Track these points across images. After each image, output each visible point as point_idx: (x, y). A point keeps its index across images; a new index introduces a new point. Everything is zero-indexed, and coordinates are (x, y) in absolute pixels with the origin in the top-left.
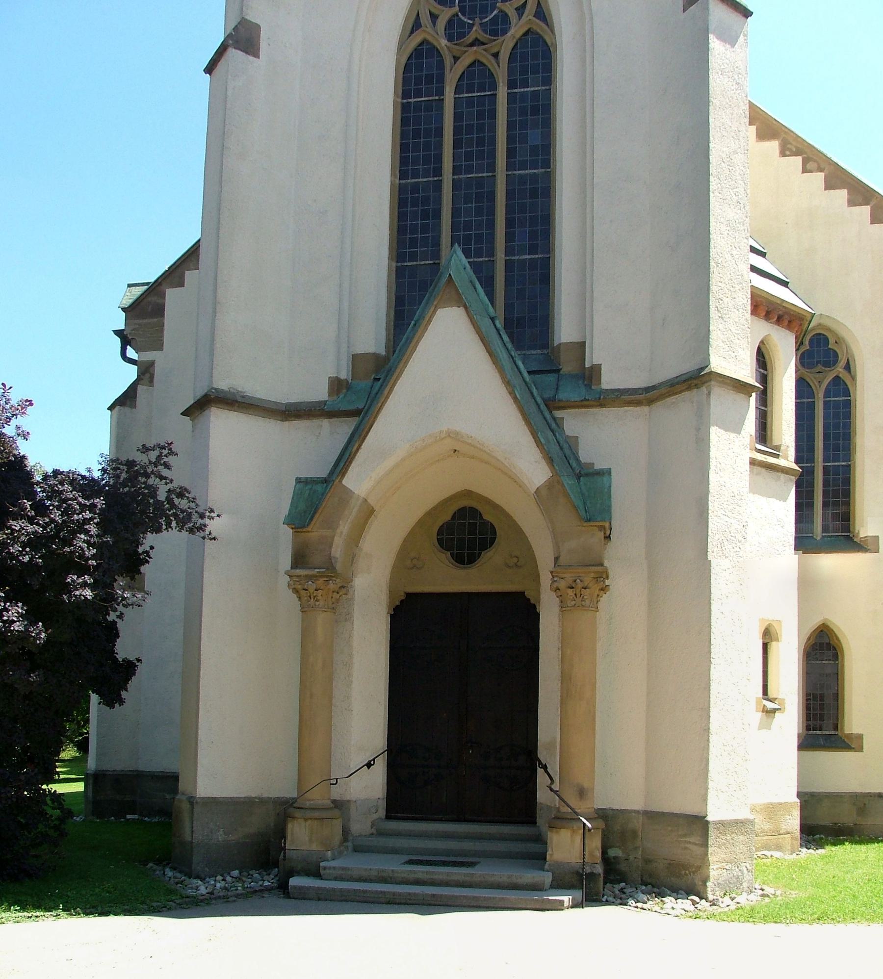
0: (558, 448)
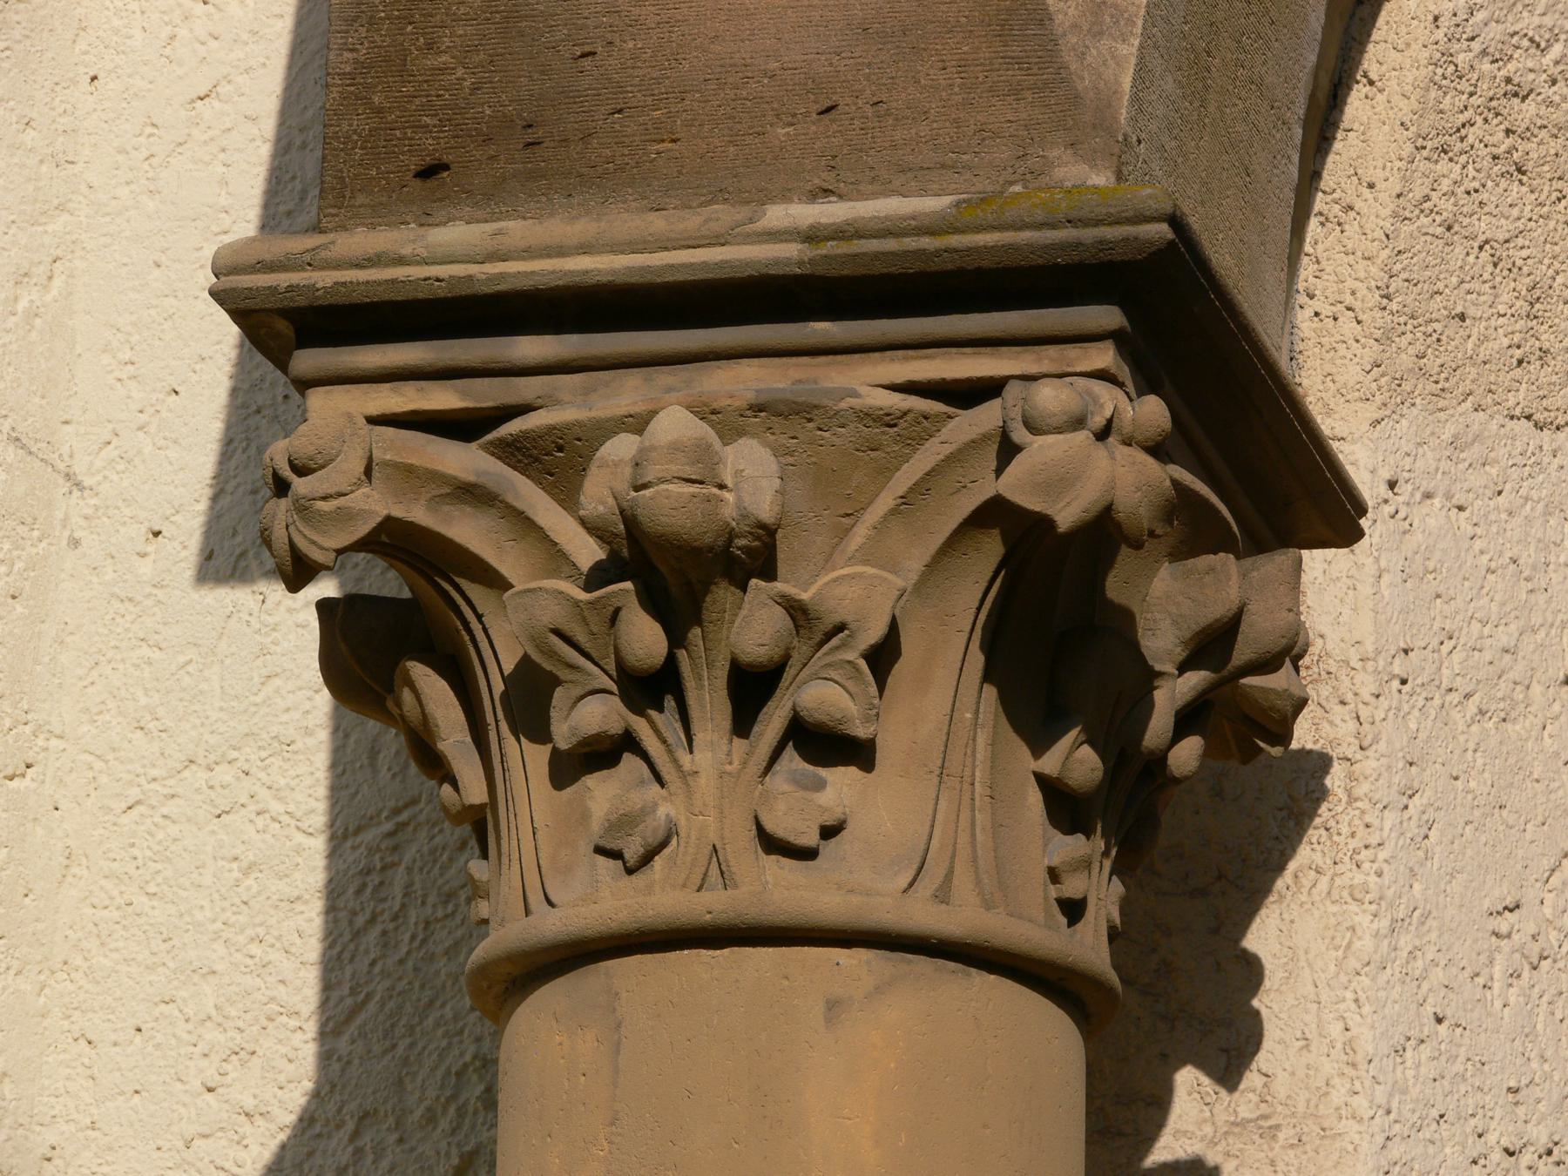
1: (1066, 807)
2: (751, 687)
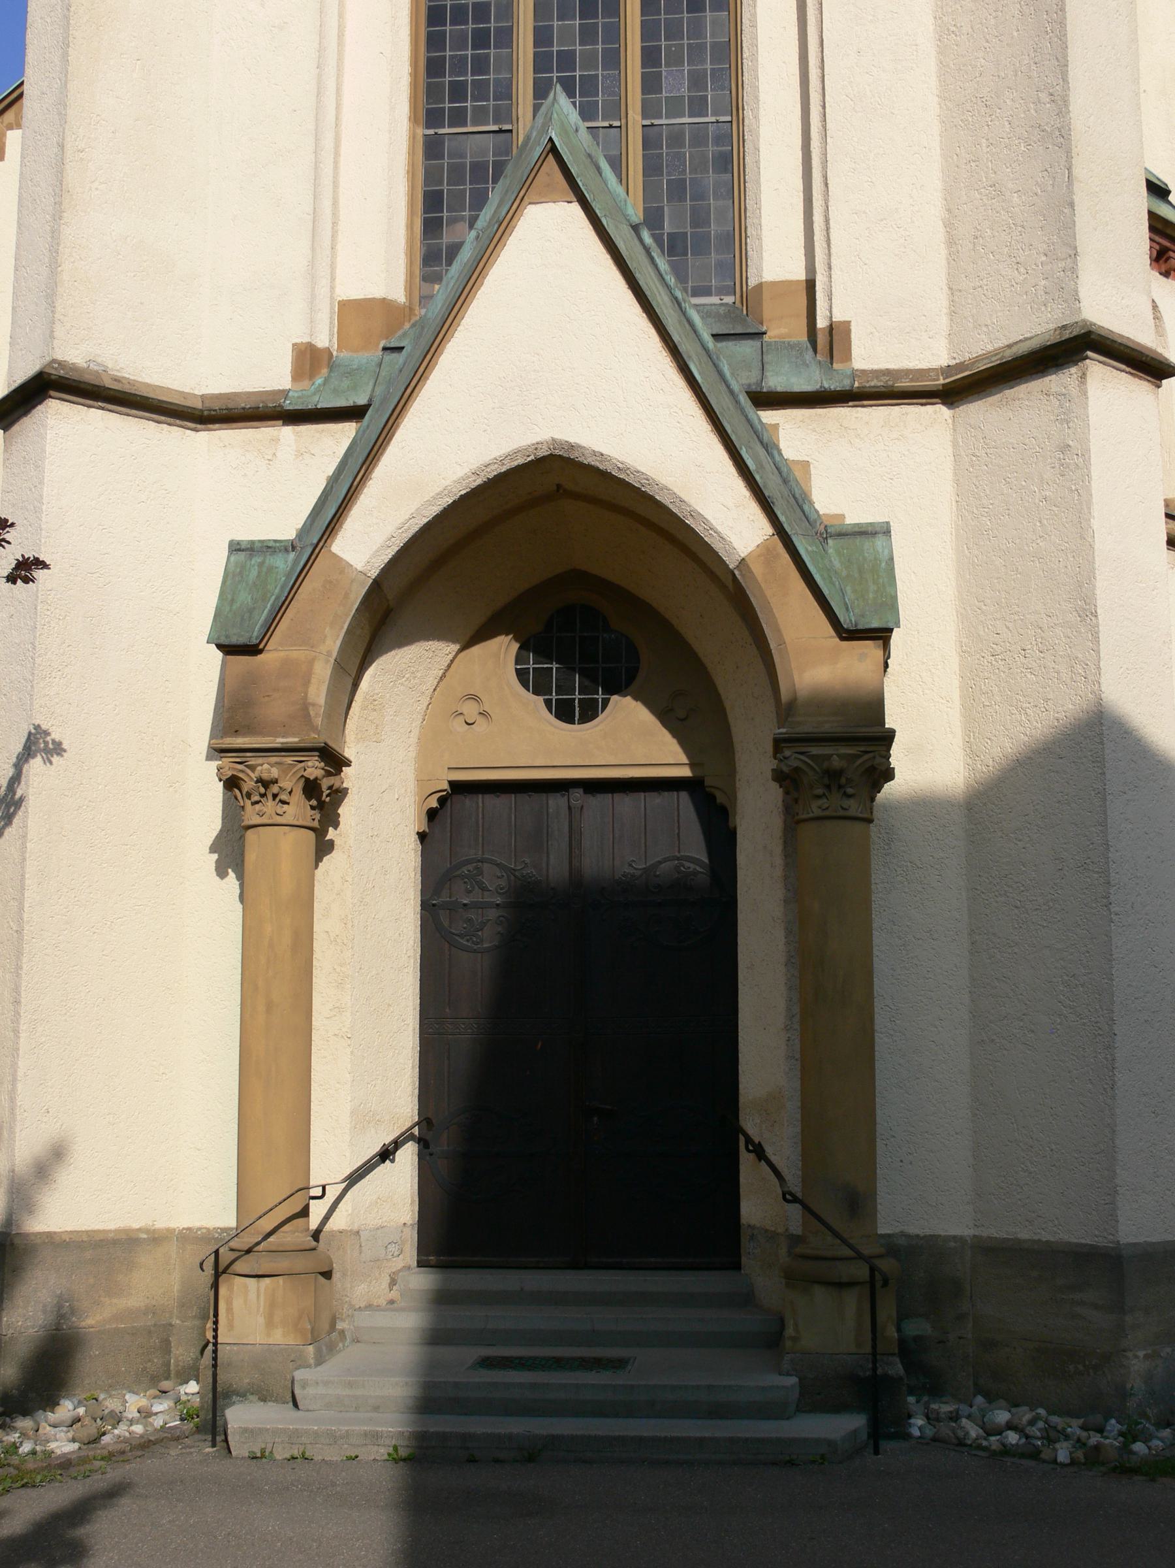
0: (779, 481)
1: (312, 808)
2: (275, 796)
